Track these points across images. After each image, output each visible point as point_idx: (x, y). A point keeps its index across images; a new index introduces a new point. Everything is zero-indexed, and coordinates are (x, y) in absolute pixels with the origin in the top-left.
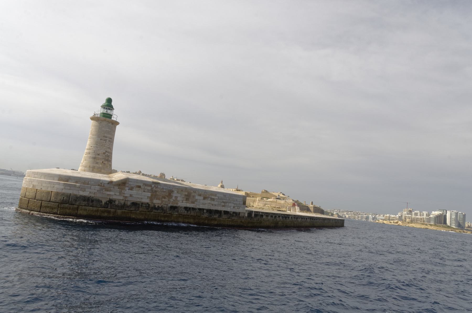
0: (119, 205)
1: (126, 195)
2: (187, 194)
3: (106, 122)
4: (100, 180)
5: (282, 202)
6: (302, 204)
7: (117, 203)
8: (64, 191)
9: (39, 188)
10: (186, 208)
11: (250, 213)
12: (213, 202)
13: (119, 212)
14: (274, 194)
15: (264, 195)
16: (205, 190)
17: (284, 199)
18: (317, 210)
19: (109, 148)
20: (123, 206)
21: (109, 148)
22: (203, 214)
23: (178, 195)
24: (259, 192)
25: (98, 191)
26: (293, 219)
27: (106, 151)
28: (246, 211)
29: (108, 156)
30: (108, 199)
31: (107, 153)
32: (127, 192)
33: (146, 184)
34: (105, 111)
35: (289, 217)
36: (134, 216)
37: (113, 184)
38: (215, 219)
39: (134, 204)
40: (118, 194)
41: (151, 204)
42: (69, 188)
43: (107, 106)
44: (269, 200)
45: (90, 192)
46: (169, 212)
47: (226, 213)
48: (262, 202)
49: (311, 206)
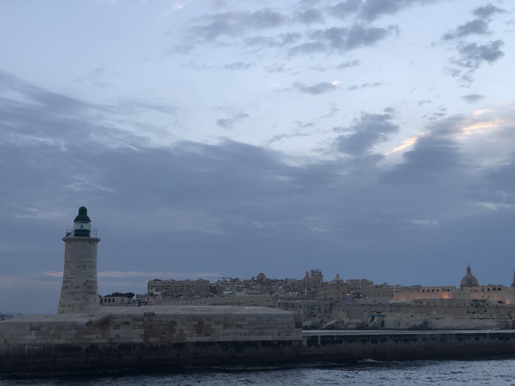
1: (110, 337)
2: (196, 323)
19: (90, 276)
21: (90, 276)
28: (304, 337)
29: (91, 287)
31: (89, 284)
32: (112, 333)
34: (79, 227)
40: (100, 336)
41: (145, 344)
42: (42, 337)
45: (66, 339)
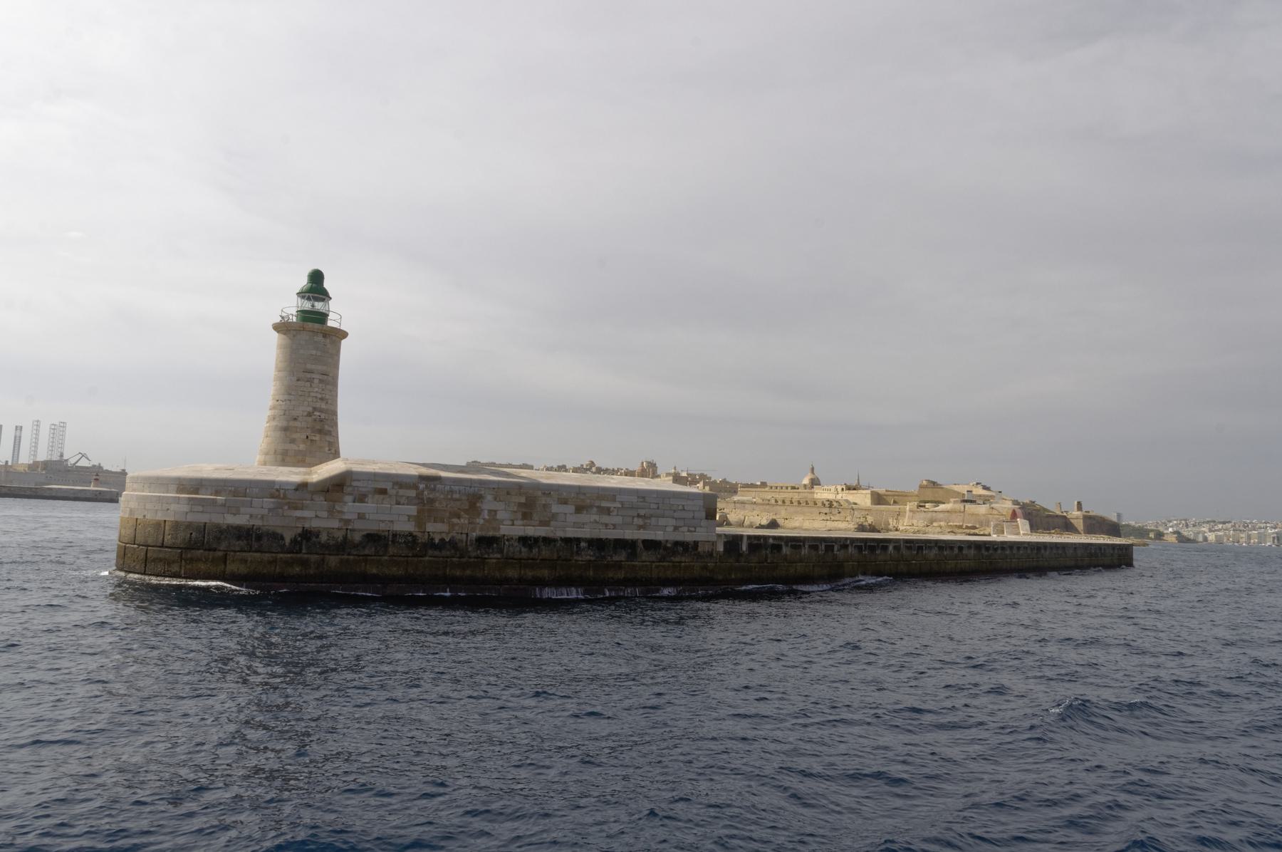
0: (332, 542)
1: (346, 517)
2: (523, 500)
3: (311, 338)
4: (273, 483)
5: (982, 509)
6: (1045, 510)
7: (324, 538)
8: (190, 518)
9: (140, 517)
10: (524, 540)
11: (733, 542)
12: (606, 519)
13: (333, 561)
14: (956, 488)
15: (929, 494)
16: (579, 487)
17: (986, 500)
18: (1095, 524)
19: (322, 399)
20: (343, 546)
21: (322, 399)
22: (578, 553)
23: (499, 506)
24: (914, 489)
25: (270, 510)
26: (904, 551)
27: (315, 409)
28: (719, 536)
30: (300, 531)
32: (350, 508)
33: (400, 482)
34: (307, 305)
35: (885, 548)
36: (374, 571)
37: (310, 488)
38: (618, 565)
39: (373, 538)
40: (325, 514)
41: (419, 535)
42: (200, 509)
43: (310, 290)
44: (942, 507)
46: (474, 554)
47: (651, 545)
48: (923, 515)
49: (1075, 515)
